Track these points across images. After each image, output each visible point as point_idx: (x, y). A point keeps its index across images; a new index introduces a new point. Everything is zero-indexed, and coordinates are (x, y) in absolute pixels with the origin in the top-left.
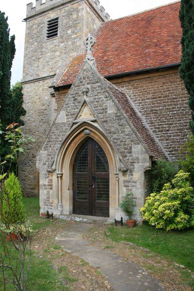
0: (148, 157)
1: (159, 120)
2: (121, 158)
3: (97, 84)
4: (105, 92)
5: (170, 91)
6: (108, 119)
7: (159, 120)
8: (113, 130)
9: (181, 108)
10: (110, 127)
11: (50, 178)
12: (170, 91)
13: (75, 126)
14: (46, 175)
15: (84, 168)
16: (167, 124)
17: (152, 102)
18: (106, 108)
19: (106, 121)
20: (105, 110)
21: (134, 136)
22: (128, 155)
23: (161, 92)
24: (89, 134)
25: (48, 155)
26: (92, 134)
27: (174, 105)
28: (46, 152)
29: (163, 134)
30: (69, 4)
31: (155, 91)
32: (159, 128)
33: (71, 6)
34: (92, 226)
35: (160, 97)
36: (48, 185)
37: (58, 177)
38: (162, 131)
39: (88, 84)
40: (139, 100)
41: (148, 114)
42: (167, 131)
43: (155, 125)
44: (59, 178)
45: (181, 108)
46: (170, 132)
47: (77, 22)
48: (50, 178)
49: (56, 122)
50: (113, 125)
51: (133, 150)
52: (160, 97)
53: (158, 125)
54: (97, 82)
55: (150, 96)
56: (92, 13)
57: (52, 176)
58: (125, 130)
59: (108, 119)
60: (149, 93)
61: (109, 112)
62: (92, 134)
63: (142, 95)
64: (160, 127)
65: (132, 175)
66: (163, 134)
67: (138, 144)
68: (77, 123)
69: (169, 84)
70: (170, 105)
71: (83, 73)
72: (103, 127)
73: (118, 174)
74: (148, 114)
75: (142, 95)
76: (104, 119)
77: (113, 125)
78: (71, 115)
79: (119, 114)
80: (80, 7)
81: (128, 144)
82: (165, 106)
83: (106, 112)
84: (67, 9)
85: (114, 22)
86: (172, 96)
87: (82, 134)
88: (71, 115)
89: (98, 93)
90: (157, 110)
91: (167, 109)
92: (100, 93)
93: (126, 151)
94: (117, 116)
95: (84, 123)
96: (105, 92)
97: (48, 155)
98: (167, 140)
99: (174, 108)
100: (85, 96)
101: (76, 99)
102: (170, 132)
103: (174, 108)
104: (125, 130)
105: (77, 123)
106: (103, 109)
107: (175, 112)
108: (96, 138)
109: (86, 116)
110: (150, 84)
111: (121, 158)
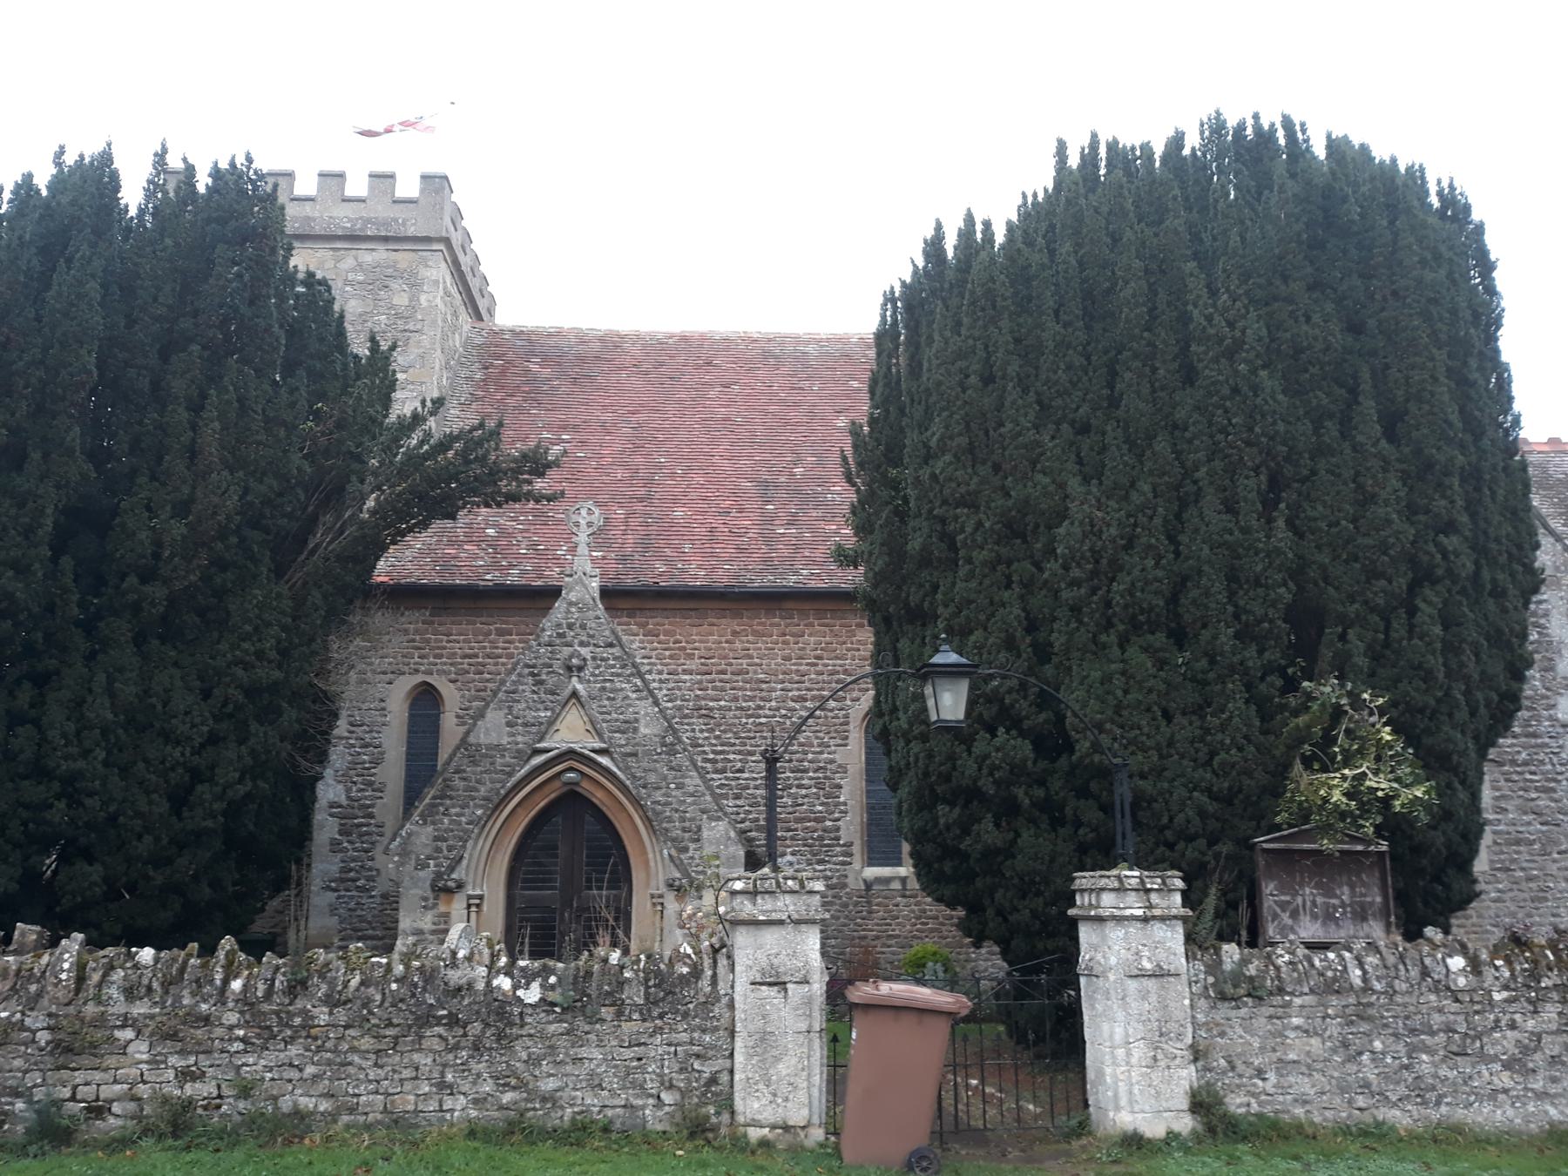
0: (742, 853)
1: (717, 737)
2: (673, 852)
3: (611, 650)
4: (632, 675)
5: (751, 657)
6: (640, 749)
7: (717, 737)
8: (652, 778)
9: (778, 709)
10: (645, 771)
11: (442, 908)
12: (751, 657)
13: (538, 760)
14: (425, 899)
15: (544, 881)
16: (740, 753)
17: (700, 682)
18: (637, 720)
19: (635, 755)
20: (630, 726)
21: (708, 798)
22: (692, 846)
23: (725, 658)
24: (577, 784)
25: (436, 839)
26: (585, 784)
27: (762, 699)
28: (430, 829)
29: (727, 778)
30: (381, 247)
31: (710, 654)
32: (714, 761)
33: (384, 255)
34: (723, 962)
35: (723, 672)
36: (433, 932)
37: (469, 906)
38: (723, 771)
39: (582, 644)
40: (660, 673)
41: (686, 716)
42: (741, 771)
43: (704, 752)
44: (473, 909)
45: (778, 709)
46: (746, 775)
47: (411, 326)
48: (442, 908)
49: (472, 739)
50: (652, 765)
51: (705, 834)
52: (723, 672)
53: (714, 752)
54: (611, 645)
55: (693, 665)
56: (454, 291)
57: (449, 902)
58: (687, 781)
59: (640, 749)
60: (691, 656)
61: (643, 730)
62: (585, 784)
63: (671, 657)
64: (719, 757)
65: (700, 898)
66: (727, 778)
67: (719, 819)
68: (547, 751)
69: (750, 638)
70: (752, 699)
71: (568, 612)
72: (626, 769)
73: (661, 896)
74: (686, 716)
75: (671, 657)
76: (628, 749)
77: (652, 765)
78: (525, 725)
79: (669, 739)
80: (425, 273)
81: (692, 819)
82: (736, 699)
83: (636, 730)
84: (368, 258)
85: (530, 344)
86: (755, 672)
87: (557, 784)
88: (525, 725)
89: (612, 674)
90: (711, 709)
91: (742, 709)
92: (618, 675)
93: (687, 835)
94: (664, 745)
95: (570, 754)
96: (632, 675)
97: (436, 839)
98: (737, 797)
99: (760, 707)
100: (574, 679)
101: (542, 682)
102: (746, 775)
103: (760, 707)
104: (687, 781)
105: (547, 751)
106: (626, 722)
107: (763, 720)
108: (598, 797)
109: (571, 732)
110: (695, 630)
111: (673, 852)
